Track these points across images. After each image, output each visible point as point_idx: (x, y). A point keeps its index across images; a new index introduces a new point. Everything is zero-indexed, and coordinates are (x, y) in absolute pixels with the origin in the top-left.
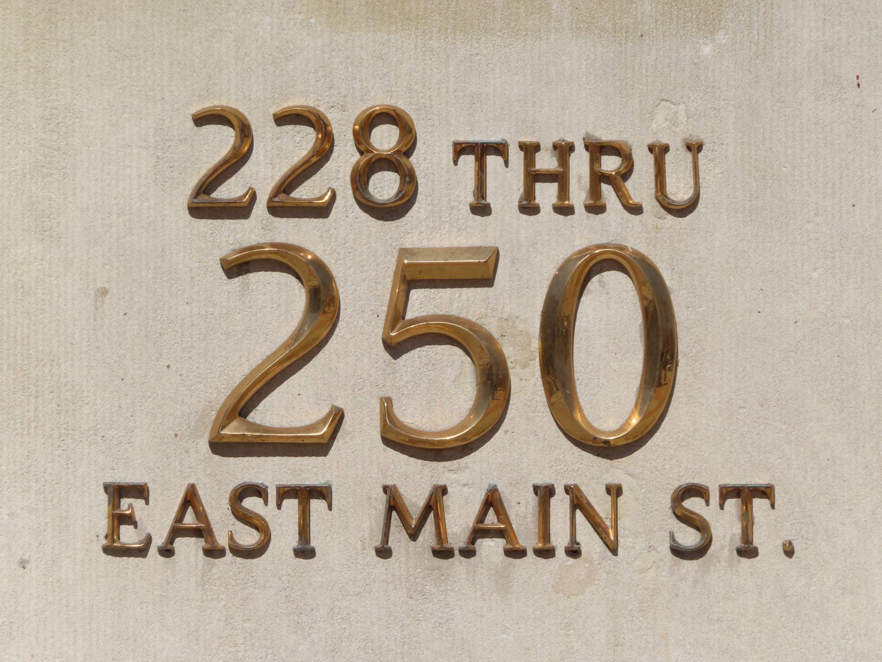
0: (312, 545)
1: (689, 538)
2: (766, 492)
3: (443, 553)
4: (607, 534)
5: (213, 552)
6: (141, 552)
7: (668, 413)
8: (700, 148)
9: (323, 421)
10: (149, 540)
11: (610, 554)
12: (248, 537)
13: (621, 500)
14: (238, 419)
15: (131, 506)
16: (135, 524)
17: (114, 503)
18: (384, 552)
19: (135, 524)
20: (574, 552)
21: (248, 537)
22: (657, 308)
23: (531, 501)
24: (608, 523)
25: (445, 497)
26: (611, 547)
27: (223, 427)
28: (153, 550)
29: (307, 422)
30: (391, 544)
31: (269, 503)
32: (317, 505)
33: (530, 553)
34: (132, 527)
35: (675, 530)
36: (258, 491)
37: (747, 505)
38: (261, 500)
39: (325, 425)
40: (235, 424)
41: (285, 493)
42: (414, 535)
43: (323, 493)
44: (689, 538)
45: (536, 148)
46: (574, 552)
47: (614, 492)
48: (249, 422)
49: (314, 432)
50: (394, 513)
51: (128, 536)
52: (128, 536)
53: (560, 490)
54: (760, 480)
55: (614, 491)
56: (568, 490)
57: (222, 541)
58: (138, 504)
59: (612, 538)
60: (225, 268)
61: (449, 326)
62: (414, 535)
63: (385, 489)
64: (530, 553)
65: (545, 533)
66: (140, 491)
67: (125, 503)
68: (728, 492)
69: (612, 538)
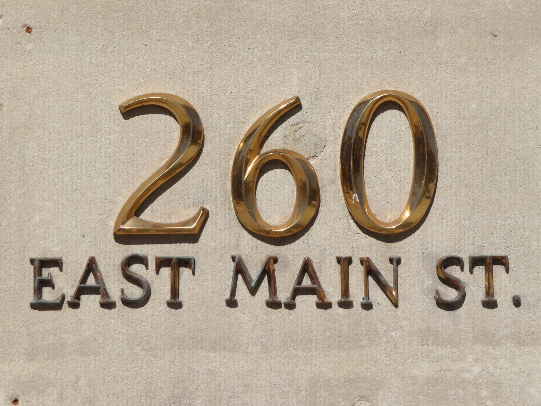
0: (180, 299)
1: (451, 294)
2: (501, 261)
3: (274, 304)
4: (392, 293)
5: (108, 305)
6: (56, 306)
7: (427, 218)
8: (399, 261)
9: (193, 220)
10: (63, 297)
11: (393, 307)
12: (135, 293)
13: (400, 268)
14: (135, 217)
15: (50, 274)
16: (53, 287)
17: (38, 272)
18: (232, 303)
19: (53, 287)
20: (367, 306)
21: (135, 293)
22: (424, 133)
23: (336, 270)
24: (391, 285)
25: (276, 265)
26: (394, 301)
27: (123, 223)
28: (65, 305)
29: (184, 219)
30: (238, 297)
31: (150, 267)
32: (185, 272)
33: (335, 305)
34: (51, 288)
35: (439, 288)
36: (142, 260)
37: (489, 273)
38: (143, 267)
39: (194, 223)
40: (130, 222)
41: (162, 263)
42: (253, 291)
43: (187, 263)
44: (451, 294)
45: (349, 261)
46: (367, 306)
47: (395, 262)
48: (142, 220)
49: (187, 226)
50: (240, 277)
51: (48, 295)
52: (48, 295)
53: (356, 262)
54: (499, 253)
55: (396, 262)
56: (362, 261)
57: (115, 296)
58: (54, 271)
59: (395, 295)
60: (123, 113)
61: (280, 155)
62: (253, 291)
63: (233, 258)
64: (335, 305)
65: (345, 291)
66: (57, 263)
67: (46, 272)
68: (476, 261)
69: (395, 295)
